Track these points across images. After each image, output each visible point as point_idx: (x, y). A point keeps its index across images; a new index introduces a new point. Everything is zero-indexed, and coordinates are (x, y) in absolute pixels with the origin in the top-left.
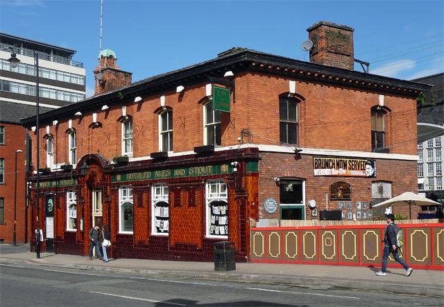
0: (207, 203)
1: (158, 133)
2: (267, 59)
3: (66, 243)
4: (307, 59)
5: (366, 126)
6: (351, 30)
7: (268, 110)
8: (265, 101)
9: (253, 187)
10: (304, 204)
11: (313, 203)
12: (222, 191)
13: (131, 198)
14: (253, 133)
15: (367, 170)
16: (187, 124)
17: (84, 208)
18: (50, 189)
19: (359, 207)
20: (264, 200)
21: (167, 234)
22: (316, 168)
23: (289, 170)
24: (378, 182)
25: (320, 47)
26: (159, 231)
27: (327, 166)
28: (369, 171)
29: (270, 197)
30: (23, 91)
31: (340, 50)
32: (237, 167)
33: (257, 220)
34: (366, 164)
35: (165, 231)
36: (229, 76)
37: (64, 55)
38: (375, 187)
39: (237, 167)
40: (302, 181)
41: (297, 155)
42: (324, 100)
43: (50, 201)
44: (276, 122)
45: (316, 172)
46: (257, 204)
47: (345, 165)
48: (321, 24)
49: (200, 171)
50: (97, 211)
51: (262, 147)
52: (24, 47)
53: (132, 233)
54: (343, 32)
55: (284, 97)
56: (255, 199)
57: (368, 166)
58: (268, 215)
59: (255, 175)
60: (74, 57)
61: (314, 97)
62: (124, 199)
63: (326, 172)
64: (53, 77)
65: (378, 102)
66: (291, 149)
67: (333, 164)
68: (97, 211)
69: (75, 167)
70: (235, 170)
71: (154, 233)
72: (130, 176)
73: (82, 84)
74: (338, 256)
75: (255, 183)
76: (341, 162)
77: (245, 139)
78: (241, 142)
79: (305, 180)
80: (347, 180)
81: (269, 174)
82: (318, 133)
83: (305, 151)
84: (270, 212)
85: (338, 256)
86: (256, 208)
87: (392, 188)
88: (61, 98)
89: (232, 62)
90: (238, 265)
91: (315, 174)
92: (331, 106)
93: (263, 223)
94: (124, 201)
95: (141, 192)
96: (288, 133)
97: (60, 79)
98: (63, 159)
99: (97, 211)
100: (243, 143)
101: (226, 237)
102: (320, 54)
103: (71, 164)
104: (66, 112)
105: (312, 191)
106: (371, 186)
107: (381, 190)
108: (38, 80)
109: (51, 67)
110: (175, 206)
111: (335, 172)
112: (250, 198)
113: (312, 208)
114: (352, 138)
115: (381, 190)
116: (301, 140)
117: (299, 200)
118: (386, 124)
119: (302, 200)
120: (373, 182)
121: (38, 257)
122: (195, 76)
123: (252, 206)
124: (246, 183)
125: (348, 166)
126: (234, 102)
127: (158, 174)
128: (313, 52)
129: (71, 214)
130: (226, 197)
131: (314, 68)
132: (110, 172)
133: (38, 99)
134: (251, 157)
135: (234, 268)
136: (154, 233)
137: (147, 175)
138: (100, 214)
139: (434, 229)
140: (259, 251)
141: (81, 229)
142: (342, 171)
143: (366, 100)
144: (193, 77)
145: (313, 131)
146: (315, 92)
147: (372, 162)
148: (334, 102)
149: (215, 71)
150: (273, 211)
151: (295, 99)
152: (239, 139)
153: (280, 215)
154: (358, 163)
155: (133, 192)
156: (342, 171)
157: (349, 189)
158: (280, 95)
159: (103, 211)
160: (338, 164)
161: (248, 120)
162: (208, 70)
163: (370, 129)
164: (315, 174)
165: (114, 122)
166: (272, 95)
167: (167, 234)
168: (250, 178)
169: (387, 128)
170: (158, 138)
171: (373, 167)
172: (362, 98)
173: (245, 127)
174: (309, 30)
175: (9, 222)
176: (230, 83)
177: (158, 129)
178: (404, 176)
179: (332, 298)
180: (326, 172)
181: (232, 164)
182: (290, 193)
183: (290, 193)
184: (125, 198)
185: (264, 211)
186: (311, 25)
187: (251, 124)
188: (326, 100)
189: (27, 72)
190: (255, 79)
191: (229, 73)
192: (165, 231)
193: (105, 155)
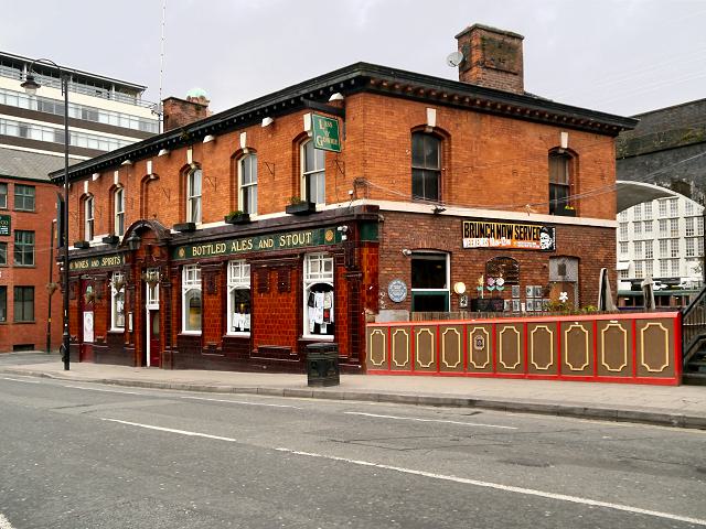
0: (305, 288)
1: (237, 186)
2: (391, 75)
3: (113, 348)
4: (453, 75)
5: (541, 175)
6: (520, 38)
7: (394, 150)
8: (393, 136)
9: (371, 263)
10: (448, 289)
11: (460, 288)
12: (326, 270)
13: (198, 283)
14: (370, 183)
15: (542, 241)
16: (277, 173)
17: (135, 306)
18: (88, 271)
19: (530, 294)
20: (388, 281)
21: (248, 334)
22: (466, 237)
23: (424, 241)
24: (559, 257)
25: (474, 59)
26: (238, 329)
27: (482, 233)
28: (546, 241)
29: (396, 277)
30: (49, 138)
31: (505, 66)
32: (347, 233)
33: (376, 311)
34: (542, 231)
35: (246, 330)
36: (336, 100)
37: (132, 91)
38: (553, 266)
39: (347, 233)
40: (445, 255)
41: (437, 214)
42: (478, 137)
43: (89, 289)
44: (405, 168)
45: (468, 242)
46: (376, 289)
47: (510, 233)
48: (476, 27)
49: (298, 240)
50: (152, 304)
51: (384, 205)
52: (74, 80)
53: (199, 332)
54: (508, 40)
55: (419, 132)
56: (373, 281)
57: (543, 235)
58: (392, 305)
59: (374, 246)
60: (144, 95)
61: (465, 133)
62: (190, 283)
63: (482, 242)
64: (113, 122)
65: (560, 142)
66: (429, 208)
67: (492, 231)
68: (153, 303)
69: (121, 238)
70: (344, 238)
71: (230, 333)
72: (196, 251)
73: (608, 309)
74: (495, 364)
75: (373, 257)
76: (505, 228)
77: (360, 192)
78: (354, 197)
79: (451, 253)
80: (513, 255)
81: (399, 244)
82: (470, 185)
83: (450, 211)
84: (397, 300)
85: (495, 364)
86: (375, 293)
87: (579, 270)
88: (93, 145)
89: (340, 79)
90: (343, 378)
91: (465, 246)
92: (489, 147)
93: (385, 317)
94: (189, 287)
95: (214, 275)
96: (428, 185)
97: (125, 124)
98: (106, 228)
99: (152, 304)
100: (356, 198)
101: (331, 337)
102: (475, 70)
103: (117, 235)
104: (105, 164)
105: (460, 270)
106: (548, 262)
107: (562, 270)
108: (68, 121)
109: (112, 109)
110: (209, 294)
111: (494, 242)
112: (367, 281)
113: (458, 296)
114: (520, 193)
115: (562, 270)
116: (445, 196)
117: (442, 284)
118: (571, 176)
119: (445, 282)
120: (551, 257)
121: (67, 368)
122: (287, 102)
123: (369, 292)
124: (361, 257)
125: (514, 233)
126: (345, 139)
127: (235, 246)
128: (464, 67)
129: (117, 306)
130: (332, 279)
131: (463, 89)
132: (170, 246)
133: (67, 149)
134: (368, 218)
135: (337, 382)
136: (230, 333)
137: (221, 248)
138: (156, 307)
139: (638, 322)
140: (378, 357)
141: (131, 328)
142: (505, 242)
143: (541, 138)
144: (284, 105)
145: (462, 182)
146: (464, 128)
147: (549, 228)
148: (495, 141)
149: (316, 93)
150: (401, 299)
151: (439, 136)
152: (351, 192)
153: (411, 304)
154: (529, 230)
155: (203, 276)
156: (505, 242)
157: (514, 268)
158: (412, 129)
159: (160, 303)
160: (499, 231)
161: (365, 164)
162: (304, 92)
163: (547, 182)
164: (465, 246)
165: (176, 173)
166: (400, 130)
167: (248, 334)
168: (366, 251)
169: (571, 181)
170: (237, 195)
171: (551, 237)
172: (535, 138)
173: (358, 174)
174: (458, 37)
175: (41, 320)
176: (340, 112)
177: (237, 182)
178: (596, 251)
179: (473, 427)
180: (482, 242)
181: (340, 228)
182: (427, 270)
183: (427, 270)
184: (191, 283)
185: (388, 299)
186: (458, 32)
187: (369, 171)
188: (483, 137)
189: (30, 106)
190: (374, 103)
191: (335, 96)
192: (246, 330)
193: (163, 221)
